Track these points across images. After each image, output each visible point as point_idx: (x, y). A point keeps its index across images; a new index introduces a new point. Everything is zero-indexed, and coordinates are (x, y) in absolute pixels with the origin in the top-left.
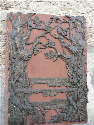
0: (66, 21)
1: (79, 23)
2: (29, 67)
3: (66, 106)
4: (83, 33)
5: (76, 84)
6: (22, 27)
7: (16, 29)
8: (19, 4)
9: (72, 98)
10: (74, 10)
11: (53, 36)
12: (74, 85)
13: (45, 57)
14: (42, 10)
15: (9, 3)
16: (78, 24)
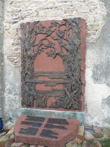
0: (63, 24)
1: (74, 24)
2: (35, 63)
3: (62, 95)
4: (78, 33)
5: (70, 77)
6: (30, 33)
7: (25, 35)
8: (31, 14)
9: (68, 89)
10: (77, 11)
11: (52, 38)
12: (69, 78)
13: (47, 55)
14: (49, 16)
15: (24, 14)
16: (73, 25)
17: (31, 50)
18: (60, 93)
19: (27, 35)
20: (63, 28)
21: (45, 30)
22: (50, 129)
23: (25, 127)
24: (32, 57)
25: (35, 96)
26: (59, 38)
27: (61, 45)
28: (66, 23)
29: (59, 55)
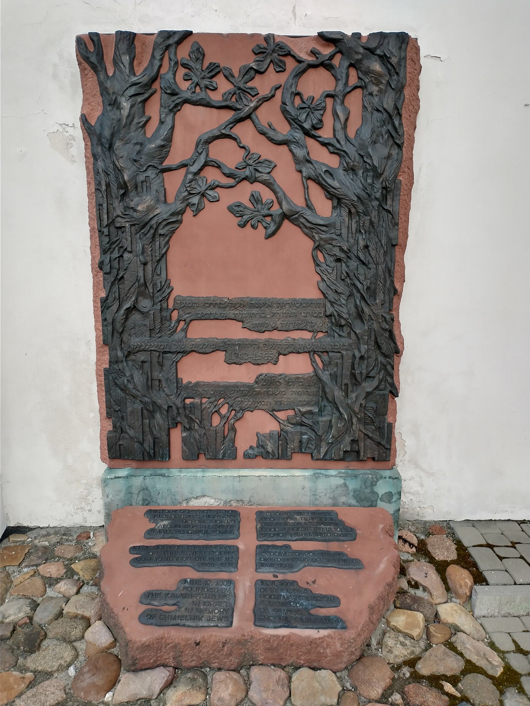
1: (377, 67)
4: (394, 113)
7: (115, 104)
9: (334, 377)
16: (373, 72)
17: (149, 188)
18: (298, 393)
19: (126, 105)
20: (316, 85)
21: (224, 86)
22: (290, 576)
23: (164, 577)
24: (156, 229)
25: (179, 413)
26: (299, 135)
27: (307, 170)
28: (332, 57)
29: (293, 222)
